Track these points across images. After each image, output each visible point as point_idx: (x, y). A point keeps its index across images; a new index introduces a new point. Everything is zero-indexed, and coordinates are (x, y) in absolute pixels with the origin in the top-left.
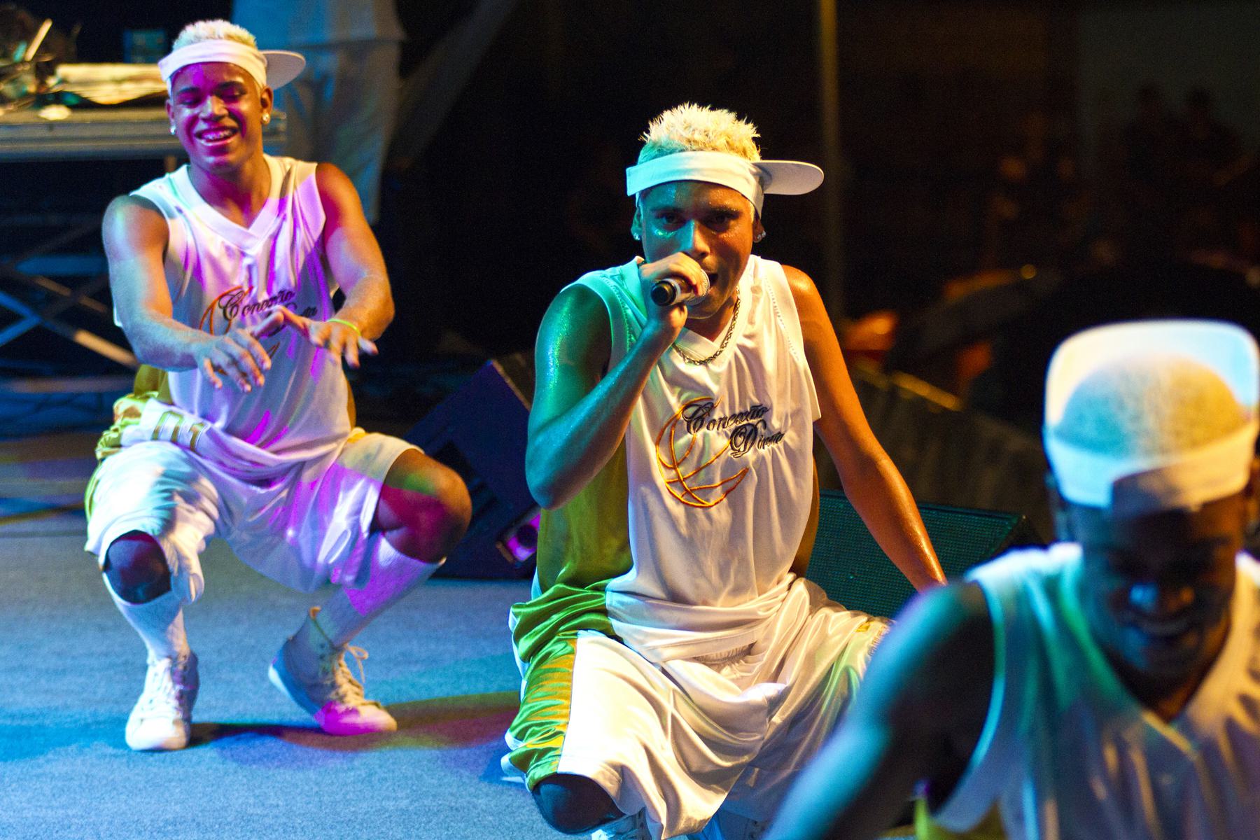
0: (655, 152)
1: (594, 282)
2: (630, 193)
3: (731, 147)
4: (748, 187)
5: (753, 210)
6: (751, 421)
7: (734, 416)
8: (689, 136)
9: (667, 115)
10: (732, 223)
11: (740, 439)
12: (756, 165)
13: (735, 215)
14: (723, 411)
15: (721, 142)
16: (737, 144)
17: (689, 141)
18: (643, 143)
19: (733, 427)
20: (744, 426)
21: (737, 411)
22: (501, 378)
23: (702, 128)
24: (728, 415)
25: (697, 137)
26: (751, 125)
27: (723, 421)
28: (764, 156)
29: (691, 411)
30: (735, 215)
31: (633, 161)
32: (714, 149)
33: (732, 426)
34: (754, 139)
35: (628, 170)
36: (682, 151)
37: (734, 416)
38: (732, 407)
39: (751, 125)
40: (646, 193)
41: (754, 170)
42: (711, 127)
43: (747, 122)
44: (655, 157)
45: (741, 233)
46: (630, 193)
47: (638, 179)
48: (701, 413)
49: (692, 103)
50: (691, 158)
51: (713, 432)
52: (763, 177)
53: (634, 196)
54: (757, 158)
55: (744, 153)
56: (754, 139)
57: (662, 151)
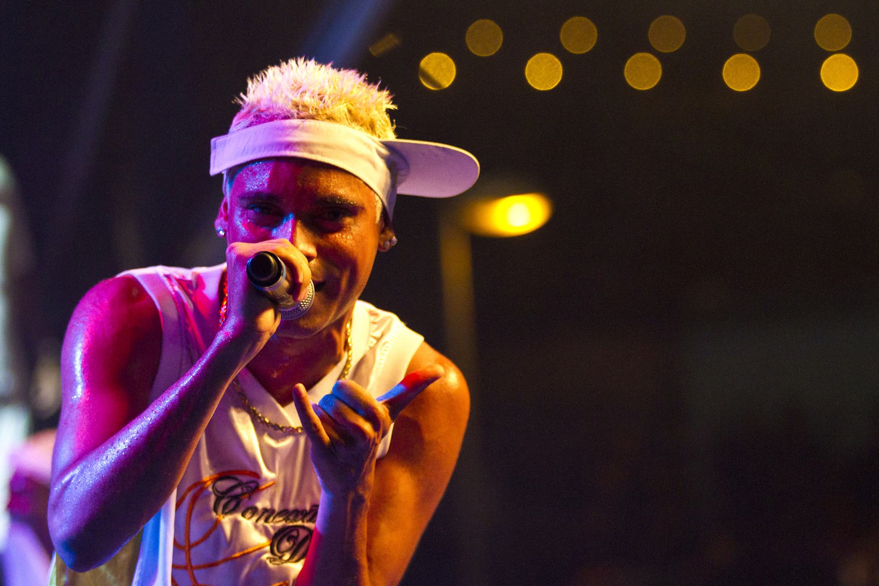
0: (251, 118)
1: (154, 279)
2: (214, 171)
3: (353, 117)
4: (375, 175)
5: (379, 205)
6: (307, 524)
7: (285, 513)
8: (297, 99)
9: (272, 72)
10: (348, 220)
11: (286, 545)
12: (387, 145)
13: (353, 210)
14: (272, 501)
15: (341, 109)
16: (362, 114)
17: (296, 105)
18: (239, 108)
19: (280, 525)
20: (296, 528)
21: (292, 506)
22: (183, 395)
23: (317, 90)
24: (277, 506)
25: (307, 99)
26: (385, 93)
27: (268, 513)
28: (399, 133)
29: (224, 485)
30: (353, 210)
31: (224, 129)
32: (330, 118)
33: (280, 523)
34: (388, 111)
35: (213, 140)
36: (286, 118)
37: (285, 513)
38: (285, 498)
39: (385, 93)
40: (233, 171)
41: (384, 151)
42: (329, 90)
43: (381, 89)
44: (250, 125)
45: (360, 238)
46: (214, 171)
47: (227, 153)
48: (238, 491)
49: (308, 58)
50: (296, 128)
51: (247, 522)
52: (396, 161)
53: (220, 175)
54: (391, 137)
55: (371, 127)
56: (388, 111)
57: (261, 117)
